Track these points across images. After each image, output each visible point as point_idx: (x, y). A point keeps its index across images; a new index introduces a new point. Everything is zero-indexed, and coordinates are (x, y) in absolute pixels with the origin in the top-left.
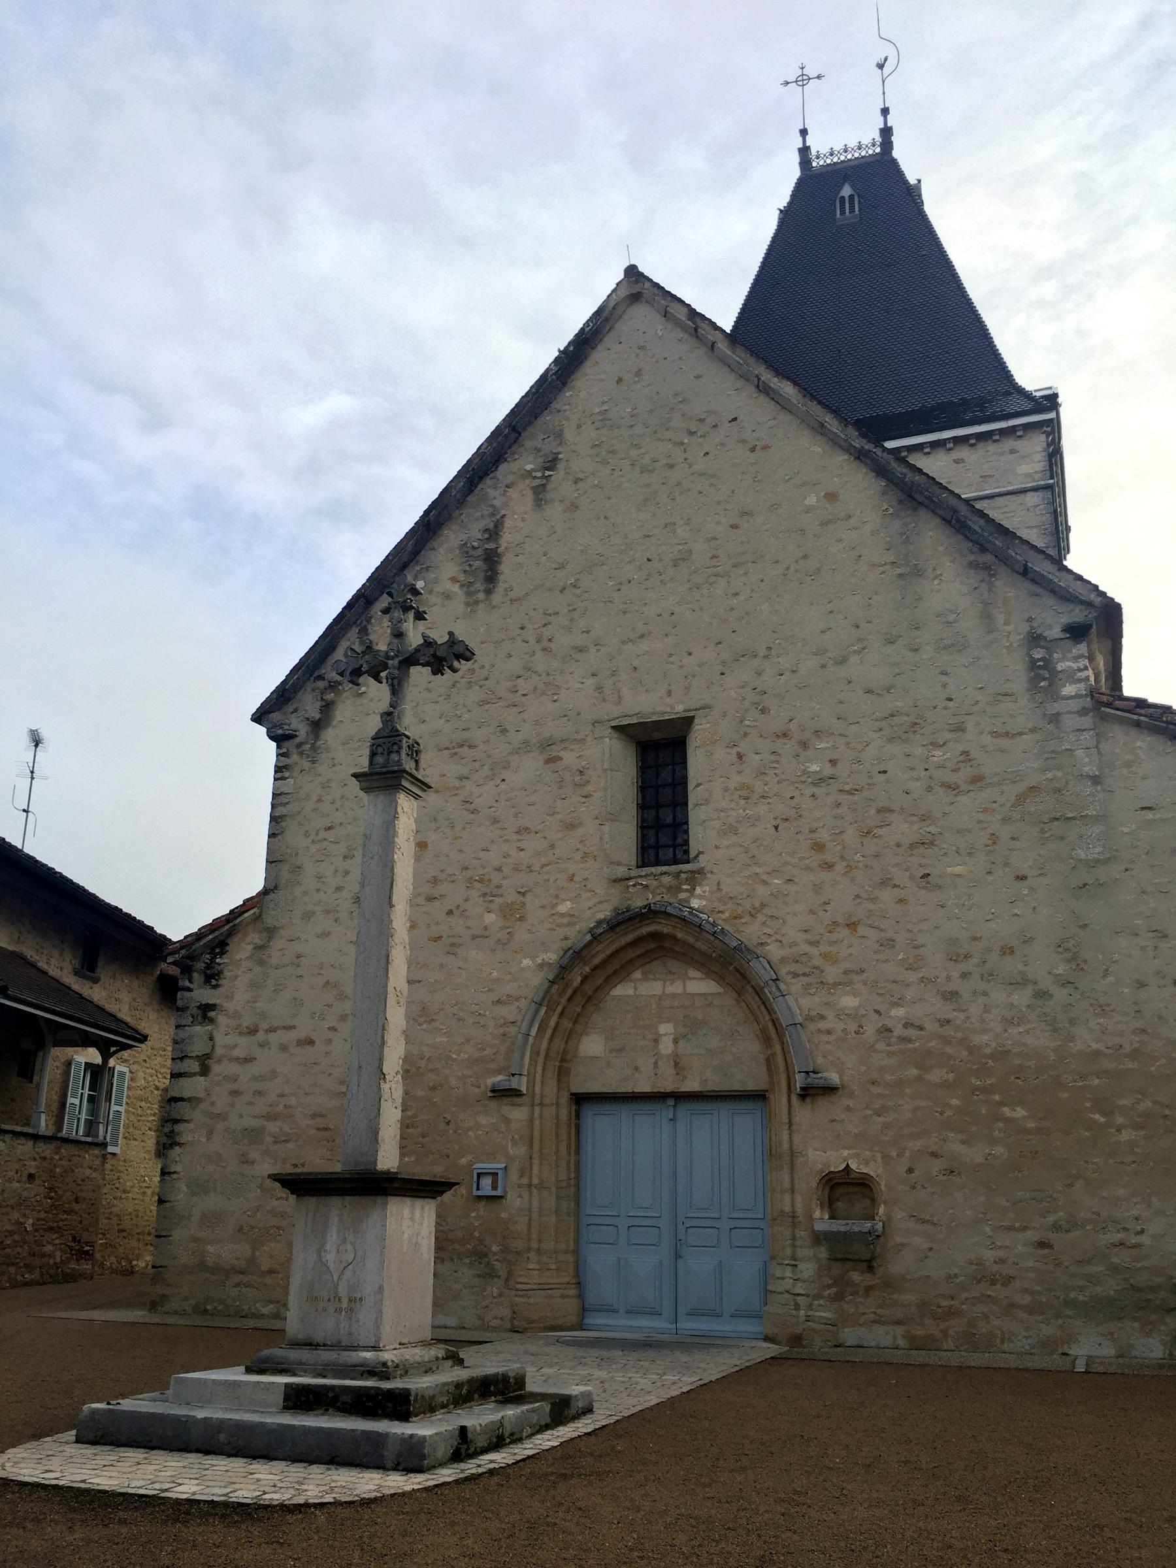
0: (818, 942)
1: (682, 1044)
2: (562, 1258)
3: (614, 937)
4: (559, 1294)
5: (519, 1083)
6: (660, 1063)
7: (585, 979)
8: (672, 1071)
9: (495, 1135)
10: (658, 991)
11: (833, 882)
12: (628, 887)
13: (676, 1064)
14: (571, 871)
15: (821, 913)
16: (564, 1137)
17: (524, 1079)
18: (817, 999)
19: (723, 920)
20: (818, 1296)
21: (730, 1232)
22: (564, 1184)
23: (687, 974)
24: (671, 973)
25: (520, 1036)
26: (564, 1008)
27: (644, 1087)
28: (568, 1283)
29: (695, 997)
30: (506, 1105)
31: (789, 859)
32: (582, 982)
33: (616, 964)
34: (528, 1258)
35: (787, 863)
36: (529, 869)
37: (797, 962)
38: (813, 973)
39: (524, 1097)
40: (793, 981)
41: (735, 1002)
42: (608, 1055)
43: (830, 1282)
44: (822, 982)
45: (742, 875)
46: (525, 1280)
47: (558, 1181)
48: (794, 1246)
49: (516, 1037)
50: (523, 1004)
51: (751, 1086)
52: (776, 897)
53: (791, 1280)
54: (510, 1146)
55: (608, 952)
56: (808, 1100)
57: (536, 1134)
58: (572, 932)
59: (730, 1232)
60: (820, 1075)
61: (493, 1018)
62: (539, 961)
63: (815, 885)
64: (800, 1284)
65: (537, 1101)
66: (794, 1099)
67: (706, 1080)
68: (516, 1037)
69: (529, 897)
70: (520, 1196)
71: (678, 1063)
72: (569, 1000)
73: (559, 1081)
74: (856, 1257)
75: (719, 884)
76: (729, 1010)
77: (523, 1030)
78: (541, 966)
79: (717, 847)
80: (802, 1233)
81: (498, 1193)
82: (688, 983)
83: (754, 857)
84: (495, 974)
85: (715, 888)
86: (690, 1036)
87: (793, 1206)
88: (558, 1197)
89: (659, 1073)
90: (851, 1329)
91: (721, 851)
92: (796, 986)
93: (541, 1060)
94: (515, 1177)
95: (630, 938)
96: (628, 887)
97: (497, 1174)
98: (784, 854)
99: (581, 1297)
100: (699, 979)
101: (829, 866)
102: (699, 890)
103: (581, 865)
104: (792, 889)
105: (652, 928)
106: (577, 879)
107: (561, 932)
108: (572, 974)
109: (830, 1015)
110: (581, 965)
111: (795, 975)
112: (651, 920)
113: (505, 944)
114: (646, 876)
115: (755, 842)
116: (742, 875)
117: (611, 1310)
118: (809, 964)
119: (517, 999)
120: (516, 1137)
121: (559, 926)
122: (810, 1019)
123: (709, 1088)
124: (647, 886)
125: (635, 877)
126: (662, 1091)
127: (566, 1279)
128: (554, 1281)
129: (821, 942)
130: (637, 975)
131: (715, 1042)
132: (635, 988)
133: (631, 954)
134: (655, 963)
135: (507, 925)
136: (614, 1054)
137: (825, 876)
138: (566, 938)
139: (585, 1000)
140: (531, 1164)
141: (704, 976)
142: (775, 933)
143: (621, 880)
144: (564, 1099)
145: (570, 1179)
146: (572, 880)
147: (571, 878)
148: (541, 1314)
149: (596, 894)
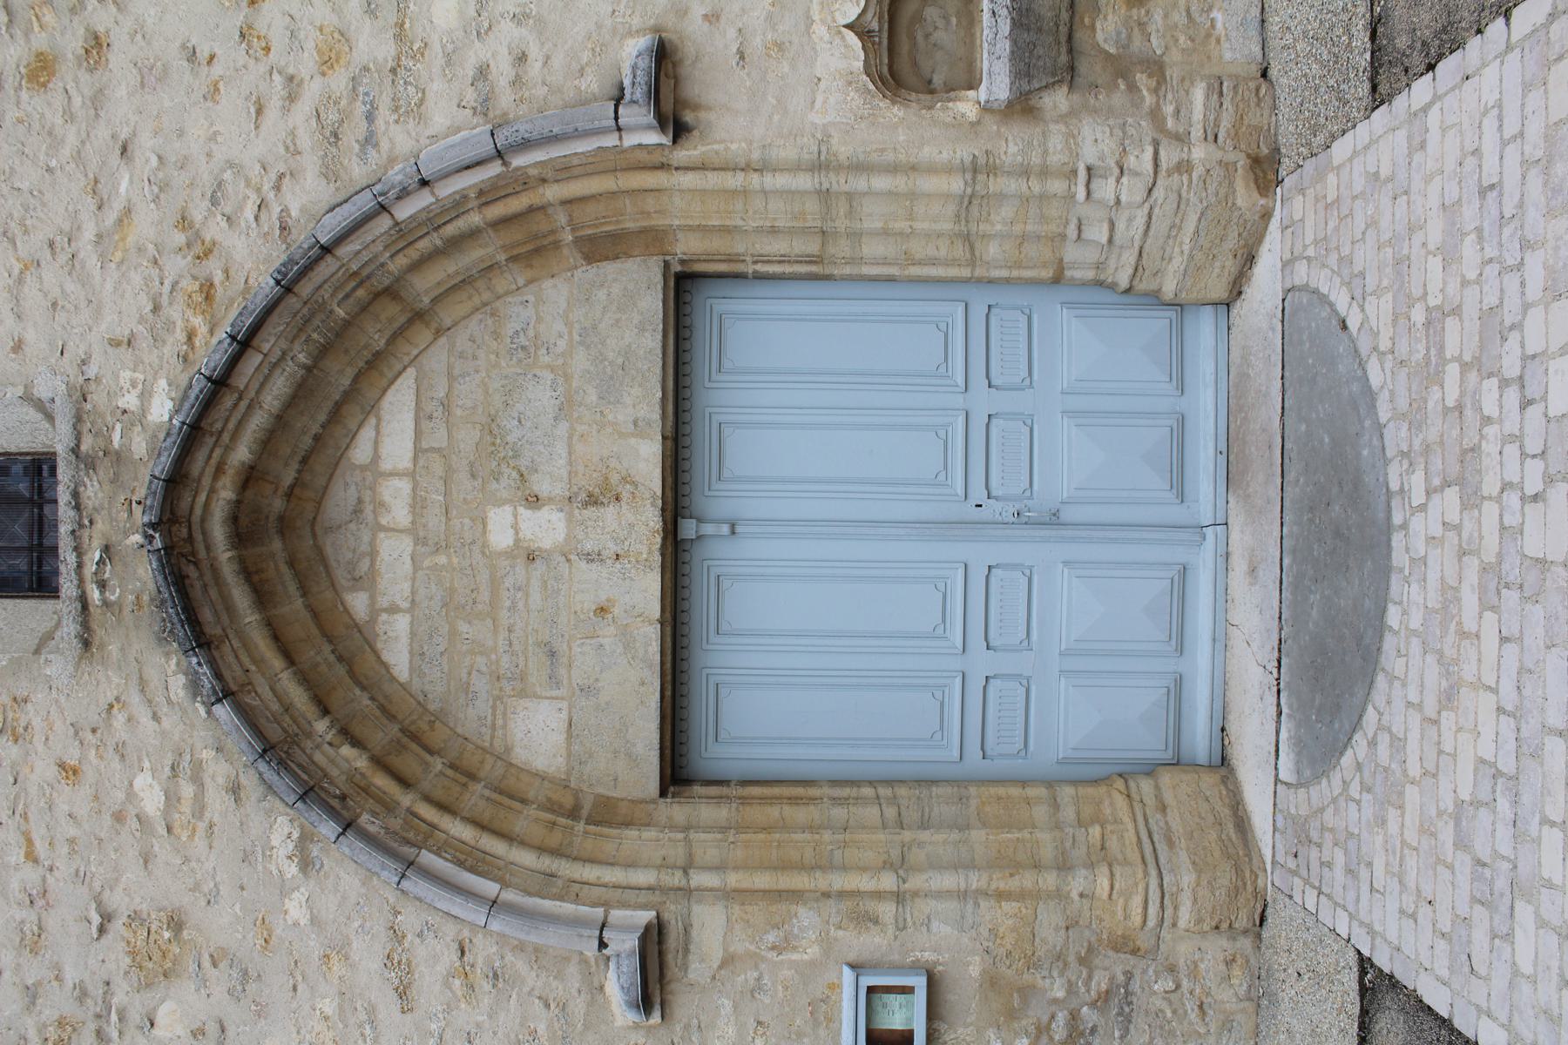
0: (291, 79)
1: (542, 486)
2: (1068, 813)
3: (236, 643)
4: (1158, 816)
5: (625, 928)
6: (588, 546)
7: (348, 735)
8: (610, 512)
9: (767, 1001)
10: (406, 545)
11: (139, 37)
12: (106, 603)
13: (592, 501)
14: (52, 772)
15: (217, 70)
16: (774, 812)
17: (617, 915)
18: (436, 86)
19: (211, 332)
20: (1156, 115)
21: (997, 388)
22: (890, 812)
23: (363, 468)
24: (358, 511)
25: (495, 926)
26: (428, 799)
27: (648, 589)
28: (1128, 796)
29: (425, 445)
30: (685, 967)
31: (66, 152)
32: (356, 743)
33: (318, 654)
34: (1081, 895)
35: (78, 156)
36: (40, 903)
37: (336, 135)
38: (367, 94)
39: (666, 916)
40: (385, 145)
41: (443, 340)
42: (562, 692)
43: (1122, 87)
44: (393, 71)
45: (98, 278)
47: (884, 827)
48: (1045, 172)
49: (502, 938)
50: (410, 919)
51: (652, 303)
52: (164, 187)
53: (1124, 180)
54: (795, 956)
55: (277, 663)
56: (688, 117)
57: (763, 881)
58: (218, 771)
59: (997, 388)
60: (627, 83)
61: (448, 1009)
62: (292, 870)
63: (143, 85)
64: (1131, 162)
65: (676, 879)
66: (682, 155)
67: (635, 423)
68: (502, 938)
69: (117, 900)
70: (928, 923)
71: (590, 495)
72: (404, 782)
73: (627, 824)
74: (1065, 16)
75: (114, 343)
76: (461, 356)
77: (477, 915)
78: (306, 864)
79: (18, 347)
80: (1013, 149)
81: (920, 983)
82: (386, 465)
83: (51, 245)
84: (328, 1006)
85: (125, 353)
86: (523, 463)
87: (949, 169)
88: (924, 825)
89: (612, 548)
90: (1225, 45)
91: (30, 336)
92: (399, 139)
93: (567, 869)
94: (877, 940)
95: (241, 597)
96: (106, 603)
97: (871, 990)
98: (53, 163)
99: (1151, 770)
100: (378, 433)
101: (96, 45)
102: (128, 397)
103: (38, 740)
104: (146, 144)
105: (219, 532)
106: (72, 758)
107: (217, 801)
108: (334, 772)
109: (476, 53)
110: (308, 744)
111: (369, 141)
112: (198, 537)
113: (245, 973)
114: (77, 549)
115: (13, 242)
116: (98, 278)
117: (1177, 690)
118: (344, 102)
119: (397, 935)
120: (771, 938)
121: (200, 809)
122: (483, 107)
123: (656, 415)
124: (107, 549)
125: (81, 581)
126: (659, 540)
127: (1120, 801)
128: (1130, 826)
129: (291, 70)
130: (358, 603)
131: (541, 397)
132: (393, 609)
133: (292, 607)
134: (329, 550)
135: (193, 967)
136: (563, 671)
137: (118, 59)
138: (235, 790)
139: (414, 746)
140: (842, 895)
141: (372, 421)
142: (258, 190)
143: (86, 625)
144: (675, 810)
145: (878, 797)
146: (75, 772)
147: (70, 772)
148: (1217, 854)
149: (117, 699)
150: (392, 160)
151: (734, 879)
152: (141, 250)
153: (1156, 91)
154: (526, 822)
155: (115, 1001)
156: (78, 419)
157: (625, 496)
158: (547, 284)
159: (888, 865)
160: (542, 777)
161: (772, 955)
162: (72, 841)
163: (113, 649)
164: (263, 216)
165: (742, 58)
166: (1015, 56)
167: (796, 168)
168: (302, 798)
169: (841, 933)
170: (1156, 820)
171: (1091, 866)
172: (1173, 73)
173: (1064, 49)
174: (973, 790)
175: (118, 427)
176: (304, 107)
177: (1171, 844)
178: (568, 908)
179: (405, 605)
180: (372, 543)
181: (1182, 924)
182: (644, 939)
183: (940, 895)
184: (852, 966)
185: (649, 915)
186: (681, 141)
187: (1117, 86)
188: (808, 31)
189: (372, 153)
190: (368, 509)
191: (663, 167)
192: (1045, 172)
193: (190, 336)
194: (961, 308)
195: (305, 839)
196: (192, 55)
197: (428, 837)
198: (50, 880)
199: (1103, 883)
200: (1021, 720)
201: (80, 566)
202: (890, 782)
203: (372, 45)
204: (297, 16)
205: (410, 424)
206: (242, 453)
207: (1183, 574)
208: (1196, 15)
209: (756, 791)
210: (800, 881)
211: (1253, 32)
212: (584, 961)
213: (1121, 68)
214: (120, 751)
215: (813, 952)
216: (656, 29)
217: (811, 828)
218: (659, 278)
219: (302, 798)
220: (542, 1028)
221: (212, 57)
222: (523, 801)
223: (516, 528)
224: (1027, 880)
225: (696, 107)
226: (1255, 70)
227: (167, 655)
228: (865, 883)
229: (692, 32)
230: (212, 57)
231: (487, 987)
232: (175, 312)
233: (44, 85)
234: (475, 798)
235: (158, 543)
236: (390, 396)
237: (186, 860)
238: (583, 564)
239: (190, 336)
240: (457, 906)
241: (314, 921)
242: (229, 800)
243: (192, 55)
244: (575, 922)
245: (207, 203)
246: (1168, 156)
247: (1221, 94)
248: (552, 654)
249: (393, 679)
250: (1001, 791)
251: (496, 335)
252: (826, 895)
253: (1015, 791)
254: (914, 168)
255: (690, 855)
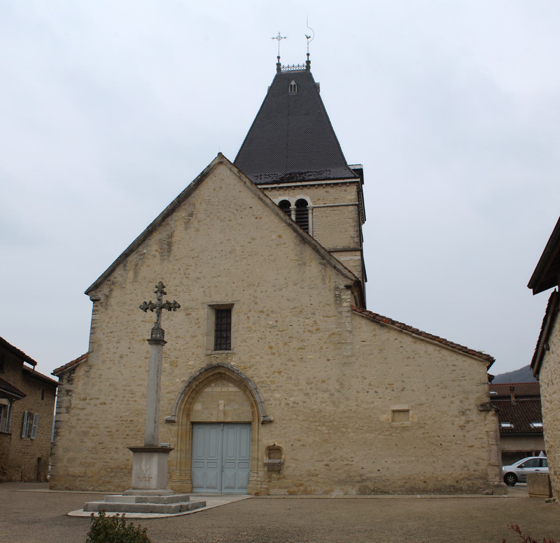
1: (226, 407)
2: (187, 472)
7: (197, 386)
8: (223, 415)
12: (211, 357)
13: (224, 413)
15: (271, 368)
16: (188, 435)
17: (176, 417)
18: (268, 394)
20: (264, 481)
22: (188, 450)
24: (223, 384)
25: (175, 404)
27: (214, 420)
30: (171, 425)
32: (196, 387)
35: (261, 352)
40: (261, 389)
48: (257, 467)
50: (177, 393)
51: (247, 420)
55: (204, 378)
56: (264, 425)
57: (180, 434)
58: (193, 371)
60: (268, 417)
62: (182, 380)
64: (259, 478)
65: (180, 424)
66: (260, 424)
69: (179, 359)
72: (191, 392)
73: (187, 418)
75: (240, 358)
79: (240, 346)
82: (229, 388)
84: (167, 384)
87: (258, 456)
88: (186, 454)
92: (262, 391)
95: (212, 374)
96: (211, 357)
99: (192, 483)
101: (274, 354)
105: (218, 371)
106: (195, 354)
107: (189, 371)
109: (272, 399)
111: (262, 387)
114: (217, 354)
117: (201, 487)
120: (173, 435)
121: (189, 369)
122: (265, 400)
124: (217, 357)
127: (188, 478)
130: (213, 385)
132: (212, 389)
138: (191, 373)
140: (178, 443)
144: (189, 423)
147: (193, 354)
150: (259, 390)
151: (180, 431)
152: (250, 360)
153: (267, 481)
154: (187, 406)
156: (232, 353)
158: (250, 407)
159: (181, 449)
160: (193, 407)
162: (186, 354)
163: (206, 358)
167: (258, 438)
171: (180, 473)
172: (269, 484)
176: (265, 379)
177: (182, 483)
182: (173, 421)
184: (170, 445)
186: (479, 411)
188: (274, 439)
192: (257, 467)
193: (240, 367)
197: (185, 395)
199: (178, 474)
202: (192, 450)
203: (273, 387)
205: (233, 391)
206: (227, 373)
207: (215, 488)
209: (191, 433)
210: (179, 438)
211: (274, 494)
212: (172, 413)
213: (270, 477)
214: (195, 359)
216: (274, 421)
217: (186, 440)
220: (164, 408)
223: (221, 404)
224: (178, 465)
225: (265, 426)
226: (269, 494)
229: (274, 425)
232: (243, 365)
234: (190, 400)
236: (237, 388)
239: (240, 367)
240: (177, 399)
241: (176, 382)
244: (176, 412)
248: (207, 408)
250: (190, 464)
252: (178, 441)
253: (190, 466)
254: (258, 451)
255: (183, 425)
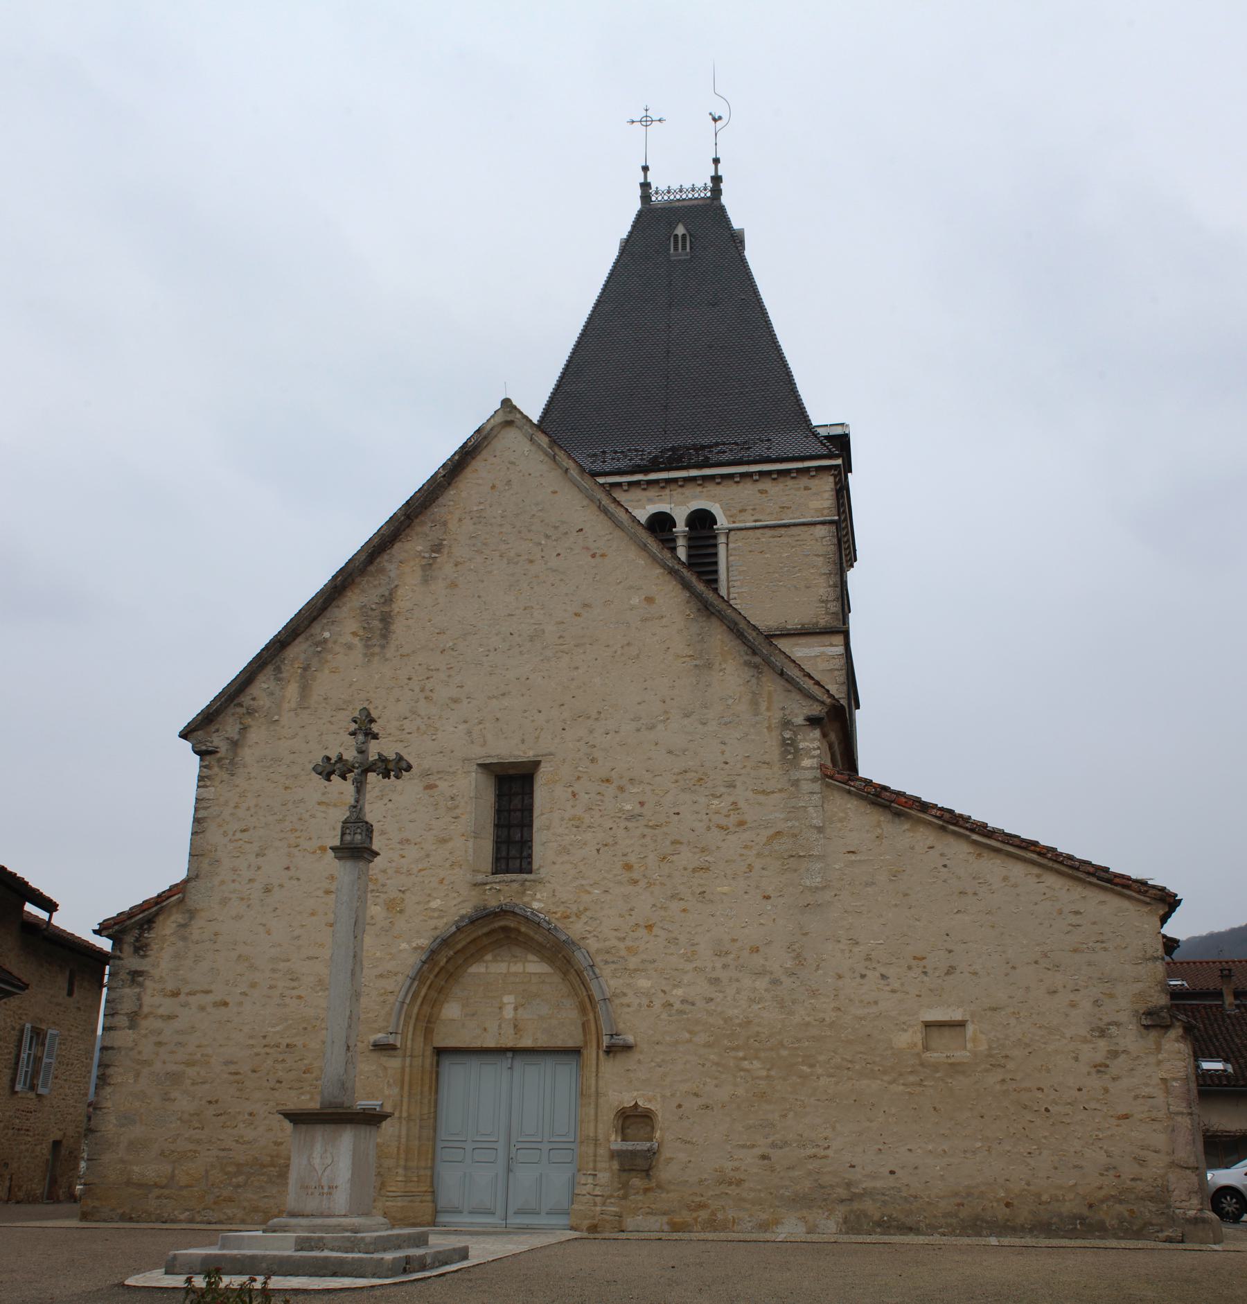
0: (624, 939)
1: (520, 1011)
2: (422, 1172)
10: (504, 971)
12: (486, 890)
13: (515, 1026)
14: (442, 876)
15: (628, 917)
17: (399, 1036)
19: (556, 919)
20: (611, 1196)
22: (425, 1117)
25: (397, 1004)
26: (432, 982)
27: (491, 1043)
32: (447, 962)
35: (604, 878)
36: (408, 873)
44: (625, 969)
46: (394, 1189)
47: (421, 1115)
48: (595, 1161)
49: (394, 1004)
50: (400, 978)
51: (570, 1043)
54: (385, 1088)
55: (468, 940)
56: (611, 1055)
57: (407, 1078)
58: (441, 923)
60: (620, 1037)
64: (598, 1188)
65: (408, 1054)
66: (601, 1053)
68: (394, 1004)
69: (408, 894)
71: (517, 1026)
73: (425, 1038)
75: (554, 891)
79: (554, 863)
80: (601, 1151)
82: (526, 964)
84: (378, 954)
87: (596, 1132)
88: (421, 1127)
92: (606, 971)
93: (412, 1021)
95: (485, 930)
96: (486, 890)
99: (434, 1201)
101: (635, 882)
103: (450, 872)
105: (502, 923)
106: (445, 882)
107: (433, 923)
110: (446, 949)
111: (606, 962)
113: (387, 931)
114: (500, 882)
118: (617, 954)
119: (396, 974)
121: (431, 918)
122: (615, 995)
123: (539, 1045)
125: (491, 883)
126: (504, 1046)
127: (424, 1189)
130: (489, 957)
132: (487, 967)
135: (389, 916)
138: (436, 928)
140: (402, 1101)
141: (539, 960)
142: (594, 931)
144: (429, 1052)
146: (442, 883)
147: (441, 881)
150: (601, 969)
151: (407, 1070)
153: (618, 1196)
155: (381, 894)
157: (516, 1036)
158: (576, 1011)
159: (409, 1115)
160: (440, 1012)
161: (386, 1081)
162: (424, 882)
163: (473, 893)
164: (587, 932)
165: (628, 1070)
166: (622, 1151)
168: (431, 950)
169: (391, 1101)
170: (418, 1199)
171: (405, 1176)
172: (623, 1202)
173: (631, 1168)
174: (431, 1143)
175: (532, 893)
178: (402, 1023)
179: (488, 971)
180: (505, 961)
181: (387, 1203)
183: (400, 1130)
184: (382, 1104)
185: (399, 1046)
187: (620, 1184)
189: (603, 964)
190: (515, 959)
191: (598, 1047)
193: (555, 913)
194: (572, 1140)
195: (422, 948)
196: (631, 910)
197: (422, 983)
198: (413, 876)
199: (400, 1179)
200: (450, 1160)
201: (496, 883)
203: (633, 962)
204: (642, 940)
205: (538, 971)
206: (523, 929)
208: (641, 1210)
209: (434, 1076)
212: (387, 1027)
213: (625, 1186)
215: (387, 1092)
217: (422, 1092)
218: (578, 1045)
219: (431, 950)
221: (631, 915)
222: (432, 1008)
224: (402, 1156)
225: (614, 1057)
226: (624, 1228)
227: (471, 909)
228: (405, 1107)
229: (635, 1056)
230: (631, 915)
231: (382, 999)
232: (562, 908)
233: (624, 868)
235: (497, 910)
237: (418, 914)
238: (498, 1023)
240: (403, 993)
242: (433, 927)
243: (631, 910)
245: (591, 916)
246: (598, 1199)
247: (615, 1216)
248: (473, 1015)
249: (468, 968)
251: (562, 996)
252: (402, 1096)
253: (430, 1156)
255: (415, 1057)
